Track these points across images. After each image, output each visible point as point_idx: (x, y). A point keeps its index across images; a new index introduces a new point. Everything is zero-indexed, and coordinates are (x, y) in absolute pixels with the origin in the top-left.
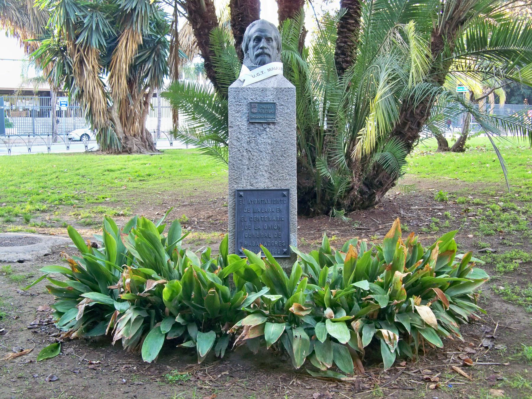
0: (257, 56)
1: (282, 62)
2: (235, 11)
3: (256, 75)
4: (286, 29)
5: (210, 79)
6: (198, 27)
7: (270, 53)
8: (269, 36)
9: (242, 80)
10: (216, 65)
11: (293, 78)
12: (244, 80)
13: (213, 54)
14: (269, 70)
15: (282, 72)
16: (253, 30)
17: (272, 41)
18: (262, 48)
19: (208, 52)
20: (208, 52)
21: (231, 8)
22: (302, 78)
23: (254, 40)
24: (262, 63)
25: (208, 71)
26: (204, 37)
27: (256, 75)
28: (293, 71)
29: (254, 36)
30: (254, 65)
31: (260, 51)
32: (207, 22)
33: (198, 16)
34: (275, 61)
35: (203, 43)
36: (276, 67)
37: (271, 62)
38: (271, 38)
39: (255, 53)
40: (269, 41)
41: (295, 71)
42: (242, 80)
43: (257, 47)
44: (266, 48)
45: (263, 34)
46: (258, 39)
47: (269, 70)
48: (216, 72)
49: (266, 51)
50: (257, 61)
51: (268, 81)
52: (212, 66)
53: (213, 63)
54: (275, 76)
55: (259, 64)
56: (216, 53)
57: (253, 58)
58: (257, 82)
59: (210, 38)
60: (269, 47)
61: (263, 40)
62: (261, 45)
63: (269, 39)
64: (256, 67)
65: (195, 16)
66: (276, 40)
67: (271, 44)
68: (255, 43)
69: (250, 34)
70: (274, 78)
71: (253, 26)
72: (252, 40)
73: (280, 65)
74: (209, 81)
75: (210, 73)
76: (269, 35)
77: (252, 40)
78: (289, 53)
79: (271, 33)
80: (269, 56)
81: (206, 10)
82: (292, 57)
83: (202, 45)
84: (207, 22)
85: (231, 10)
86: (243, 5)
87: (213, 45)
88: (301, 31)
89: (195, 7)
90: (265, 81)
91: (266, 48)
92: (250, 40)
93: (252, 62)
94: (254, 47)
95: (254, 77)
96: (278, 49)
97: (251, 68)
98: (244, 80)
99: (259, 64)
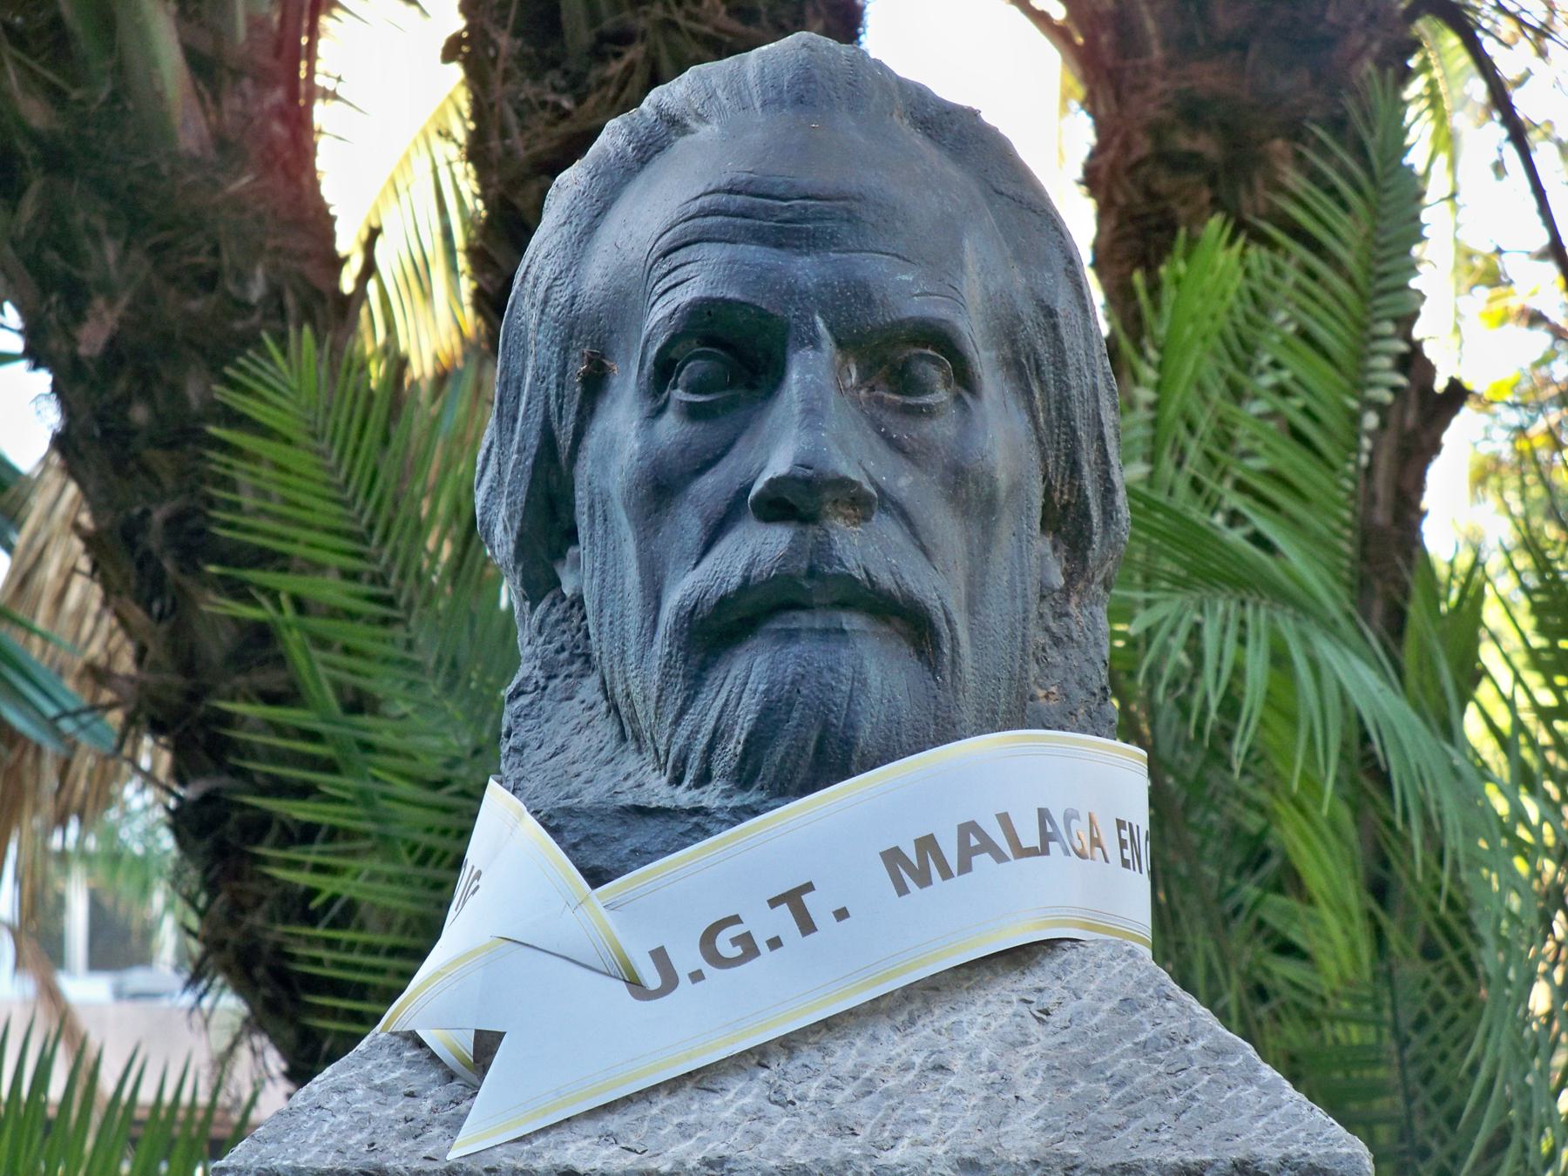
0: (714, 633)
1: (1128, 731)
2: (524, 110)
3: (687, 958)
4: (1199, 361)
5: (244, 984)
6: (92, 338)
7: (936, 587)
8: (917, 307)
9: (448, 1040)
10: (301, 811)
11: (1285, 969)
12: (486, 1045)
13: (270, 679)
14: (914, 865)
15: (1131, 899)
16: (650, 211)
17: (964, 378)
18: (788, 503)
19: (216, 646)
20: (216, 646)
21: (477, 78)
22: (1412, 969)
23: (663, 372)
24: (806, 752)
25: (211, 887)
26: (157, 458)
27: (687, 958)
28: (1290, 881)
29: (659, 313)
30: (658, 790)
31: (759, 547)
32: (209, 281)
33: (85, 213)
34: (1018, 712)
35: (154, 540)
36: (1051, 814)
37: (946, 732)
38: (941, 342)
39: (681, 589)
40: (905, 381)
41: (1314, 879)
42: (448, 1040)
43: (711, 486)
44: (861, 503)
45: (805, 269)
46: (730, 357)
47: (914, 865)
48: (301, 907)
49: (862, 548)
50: (711, 703)
51: (893, 1047)
52: (261, 825)
53: (280, 788)
54: (1019, 957)
55: (744, 776)
56: (316, 670)
57: (643, 669)
58: (703, 1079)
59: (241, 472)
60: (904, 483)
61: (810, 371)
62: (777, 457)
63: (903, 361)
64: (698, 823)
65: (54, 213)
66: (1022, 368)
67: (943, 429)
68: (670, 427)
69: (596, 274)
70: (1009, 990)
71: (648, 150)
72: (627, 381)
73: (1110, 780)
74: (229, 1006)
75: (236, 910)
76: (907, 293)
77: (627, 381)
78: (1231, 643)
79: (942, 265)
80: (913, 624)
81: (186, 122)
82: (1281, 706)
83: (145, 561)
84: (209, 281)
85: (481, 110)
86: (624, 38)
87: (265, 558)
88: (1386, 378)
89: (56, 96)
90: (845, 1056)
91: (861, 503)
92: (596, 383)
93: (628, 735)
94: (661, 488)
95: (655, 979)
96: (1066, 522)
97: (601, 843)
98: (486, 1045)
99: (744, 776)
